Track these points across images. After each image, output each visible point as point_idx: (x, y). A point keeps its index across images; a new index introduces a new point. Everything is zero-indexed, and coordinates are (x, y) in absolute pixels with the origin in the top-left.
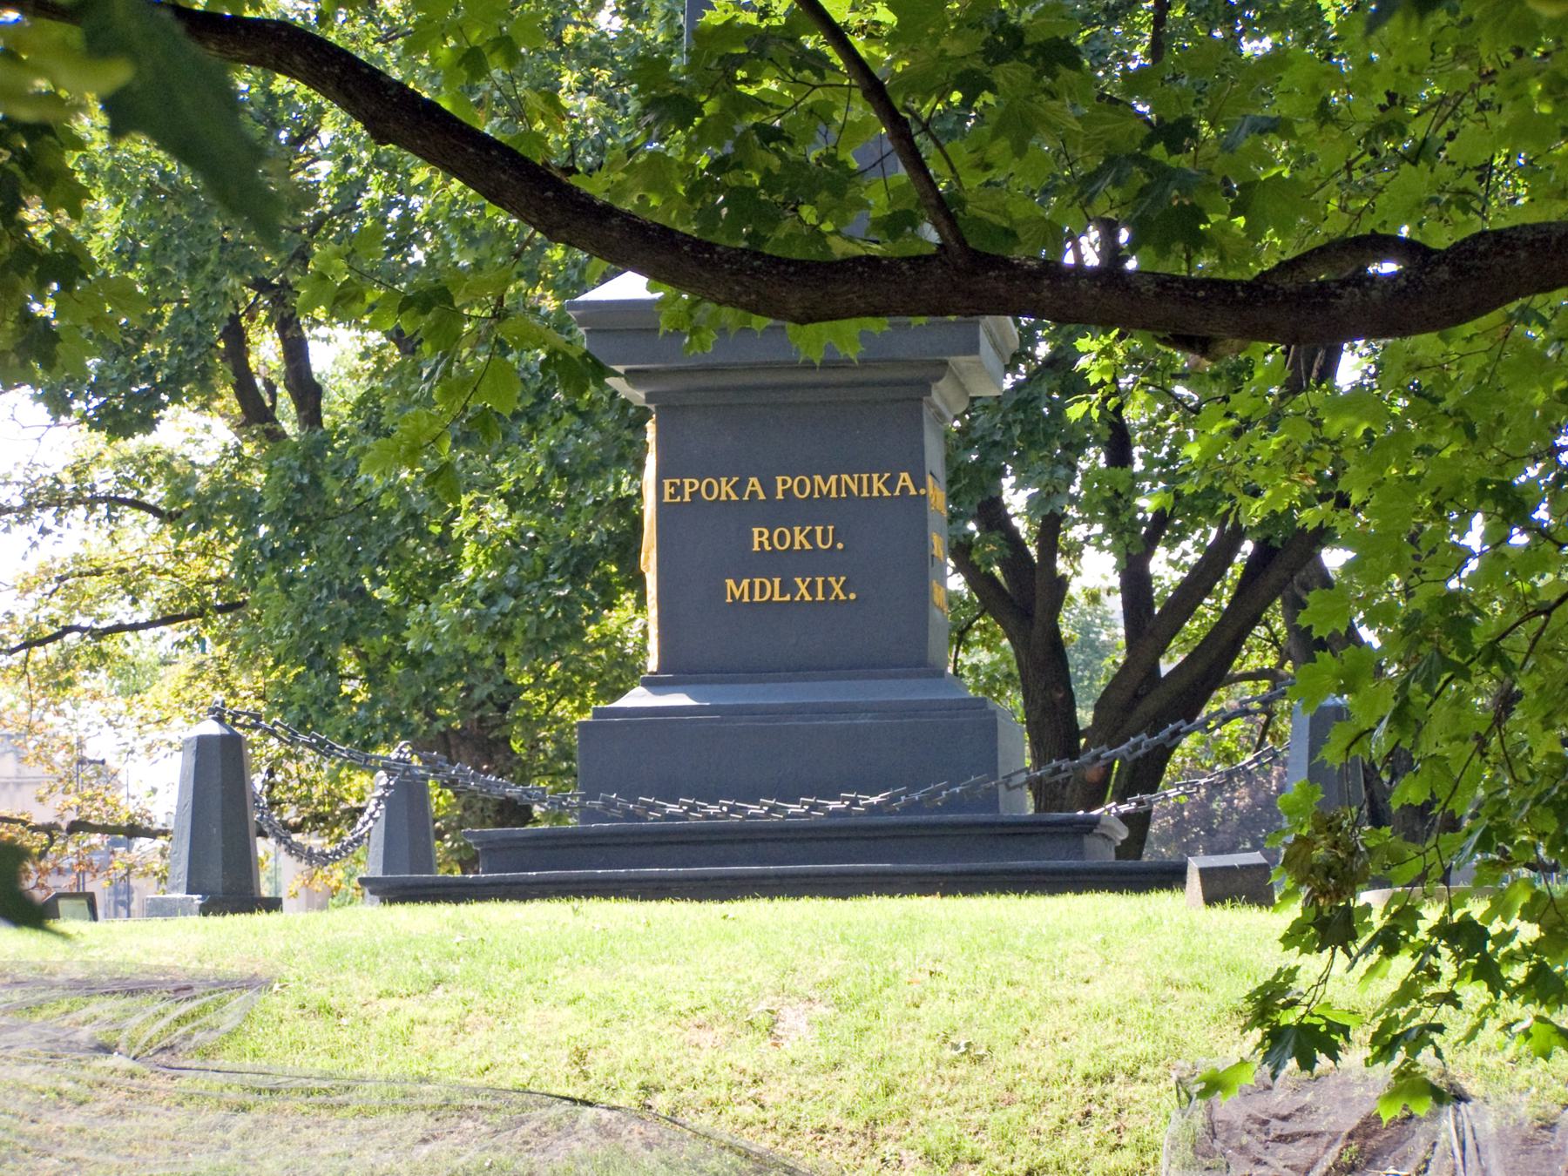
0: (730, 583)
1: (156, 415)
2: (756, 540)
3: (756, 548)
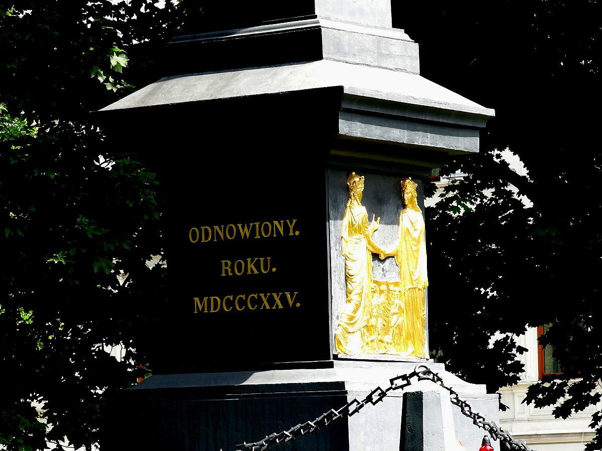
0: (197, 299)
1: (593, 421)
2: (224, 268)
3: (224, 274)
